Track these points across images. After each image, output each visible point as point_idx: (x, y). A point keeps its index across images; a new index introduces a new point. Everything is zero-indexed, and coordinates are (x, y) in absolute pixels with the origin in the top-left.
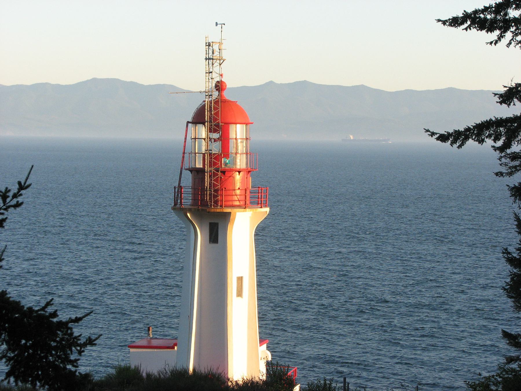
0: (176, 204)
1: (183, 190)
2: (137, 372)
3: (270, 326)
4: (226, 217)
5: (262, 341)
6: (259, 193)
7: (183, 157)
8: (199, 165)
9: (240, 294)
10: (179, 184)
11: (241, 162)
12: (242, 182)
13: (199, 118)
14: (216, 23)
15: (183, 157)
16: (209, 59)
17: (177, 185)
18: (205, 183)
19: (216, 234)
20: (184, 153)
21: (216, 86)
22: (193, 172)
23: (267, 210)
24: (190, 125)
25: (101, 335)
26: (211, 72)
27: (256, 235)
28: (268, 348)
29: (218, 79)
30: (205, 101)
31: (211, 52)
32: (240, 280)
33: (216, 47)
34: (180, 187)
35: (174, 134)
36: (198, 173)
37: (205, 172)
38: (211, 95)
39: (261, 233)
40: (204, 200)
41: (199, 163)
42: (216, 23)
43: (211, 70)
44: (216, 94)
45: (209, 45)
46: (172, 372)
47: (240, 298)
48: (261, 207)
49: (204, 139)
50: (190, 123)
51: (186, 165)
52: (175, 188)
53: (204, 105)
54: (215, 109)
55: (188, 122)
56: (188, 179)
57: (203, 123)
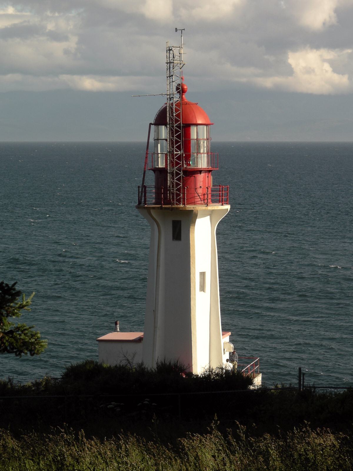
0: (140, 203)
1: (147, 189)
2: (101, 366)
3: (234, 309)
4: (191, 217)
5: (225, 330)
6: (220, 196)
7: (146, 158)
8: (161, 165)
9: (202, 288)
10: (143, 183)
11: (203, 162)
12: (204, 181)
13: (161, 119)
14: (176, 29)
15: (146, 158)
16: (170, 63)
17: (140, 184)
18: (167, 183)
19: (180, 229)
20: (147, 154)
21: (177, 89)
22: (156, 172)
23: (228, 207)
24: (153, 127)
25: (33, 327)
26: (172, 76)
27: (217, 234)
28: (232, 341)
29: (179, 82)
30: (166, 104)
31: (171, 56)
32: (203, 274)
33: (176, 51)
34: (144, 187)
35: (135, 130)
36: (161, 173)
37: (167, 172)
38: (173, 98)
39: (223, 233)
40: (167, 199)
41: (162, 163)
42: (176, 29)
43: (172, 74)
44: (176, 98)
45: (170, 50)
46: (116, 366)
47: (202, 292)
48: (222, 205)
49: (166, 140)
50: (153, 124)
51: (150, 166)
52: (139, 187)
53: (166, 108)
54: (177, 110)
55: (151, 124)
56: (151, 179)
57: (165, 124)
